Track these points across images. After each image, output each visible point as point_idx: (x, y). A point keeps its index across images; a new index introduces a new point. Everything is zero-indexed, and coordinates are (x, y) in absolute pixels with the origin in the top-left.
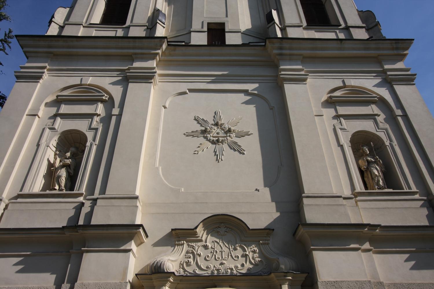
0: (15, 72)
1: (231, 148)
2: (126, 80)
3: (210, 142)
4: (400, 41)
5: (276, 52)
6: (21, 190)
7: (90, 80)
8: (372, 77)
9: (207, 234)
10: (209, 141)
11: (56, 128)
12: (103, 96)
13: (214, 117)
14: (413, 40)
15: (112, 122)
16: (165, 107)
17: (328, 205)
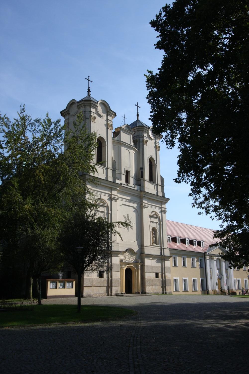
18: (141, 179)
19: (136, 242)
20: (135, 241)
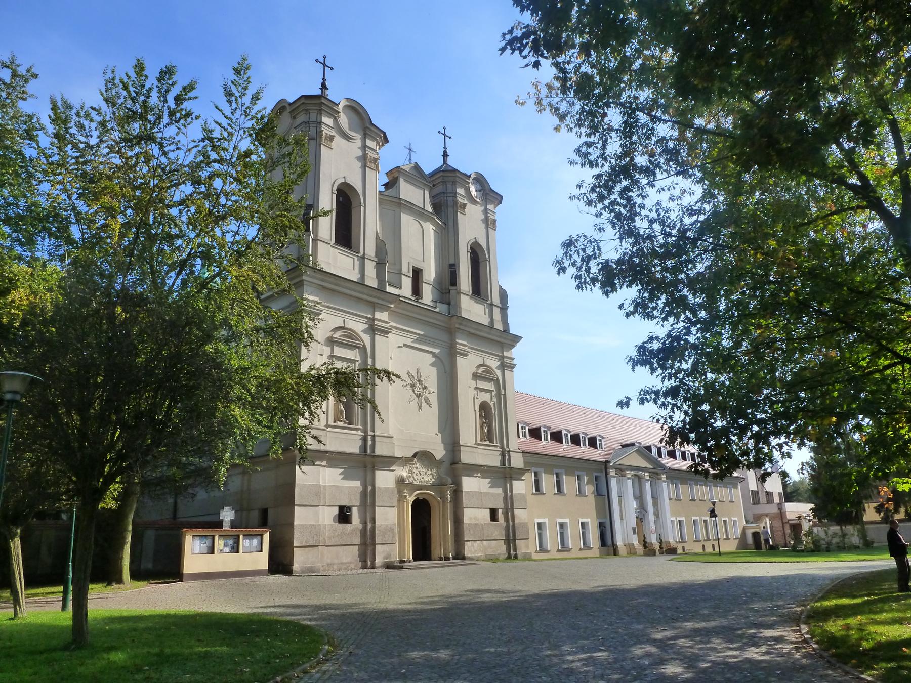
18: (451, 288)
19: (440, 435)
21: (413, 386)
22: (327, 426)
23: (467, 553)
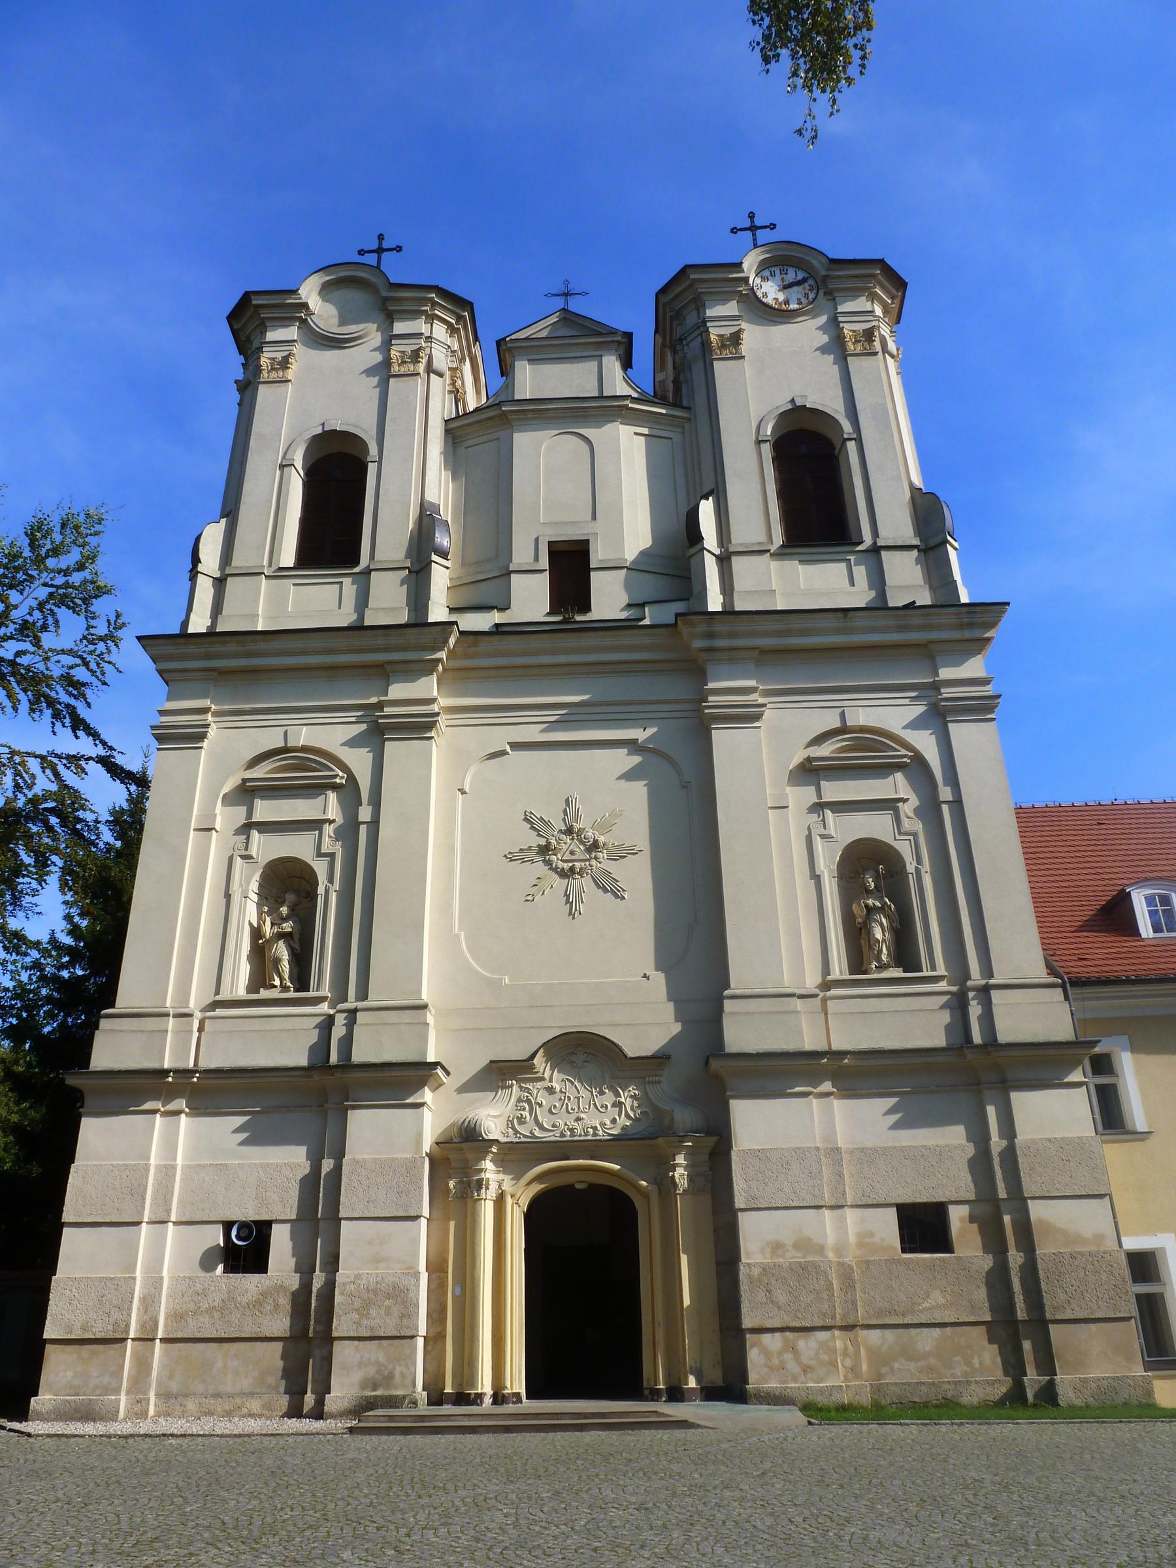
0: (153, 728)
1: (598, 886)
2: (378, 732)
3: (557, 873)
4: (978, 609)
5: (698, 644)
6: (217, 992)
7: (304, 735)
8: (907, 701)
9: (552, 1069)
10: (555, 870)
11: (254, 855)
12: (336, 776)
13: (565, 811)
14: (1008, 604)
15: (359, 836)
16: (463, 792)
17: (768, 1013)
19: (659, 978)
20: (651, 972)
21: (545, 850)
22: (826, 985)
23: (758, 1376)
